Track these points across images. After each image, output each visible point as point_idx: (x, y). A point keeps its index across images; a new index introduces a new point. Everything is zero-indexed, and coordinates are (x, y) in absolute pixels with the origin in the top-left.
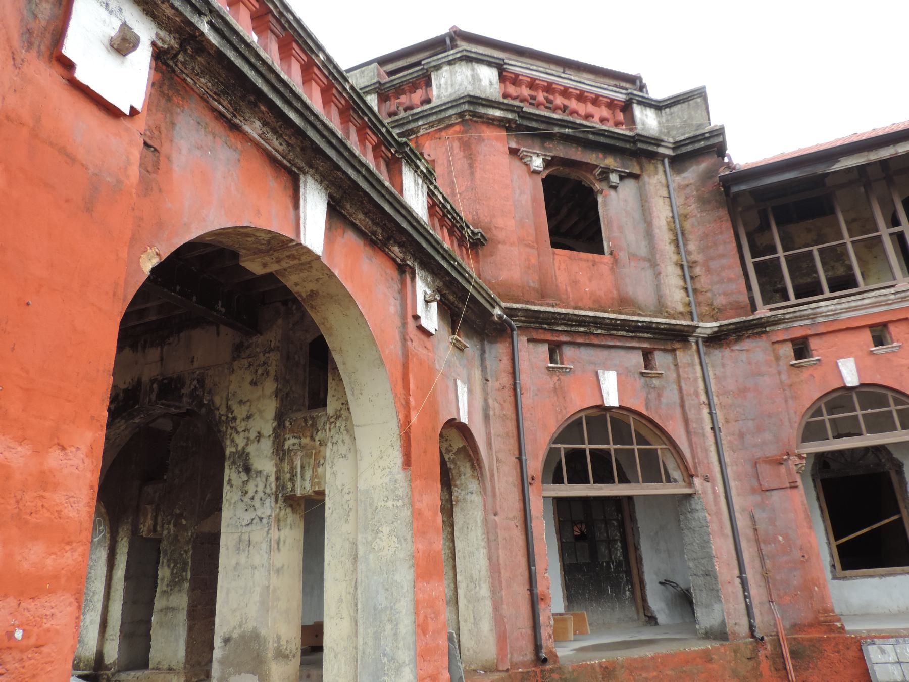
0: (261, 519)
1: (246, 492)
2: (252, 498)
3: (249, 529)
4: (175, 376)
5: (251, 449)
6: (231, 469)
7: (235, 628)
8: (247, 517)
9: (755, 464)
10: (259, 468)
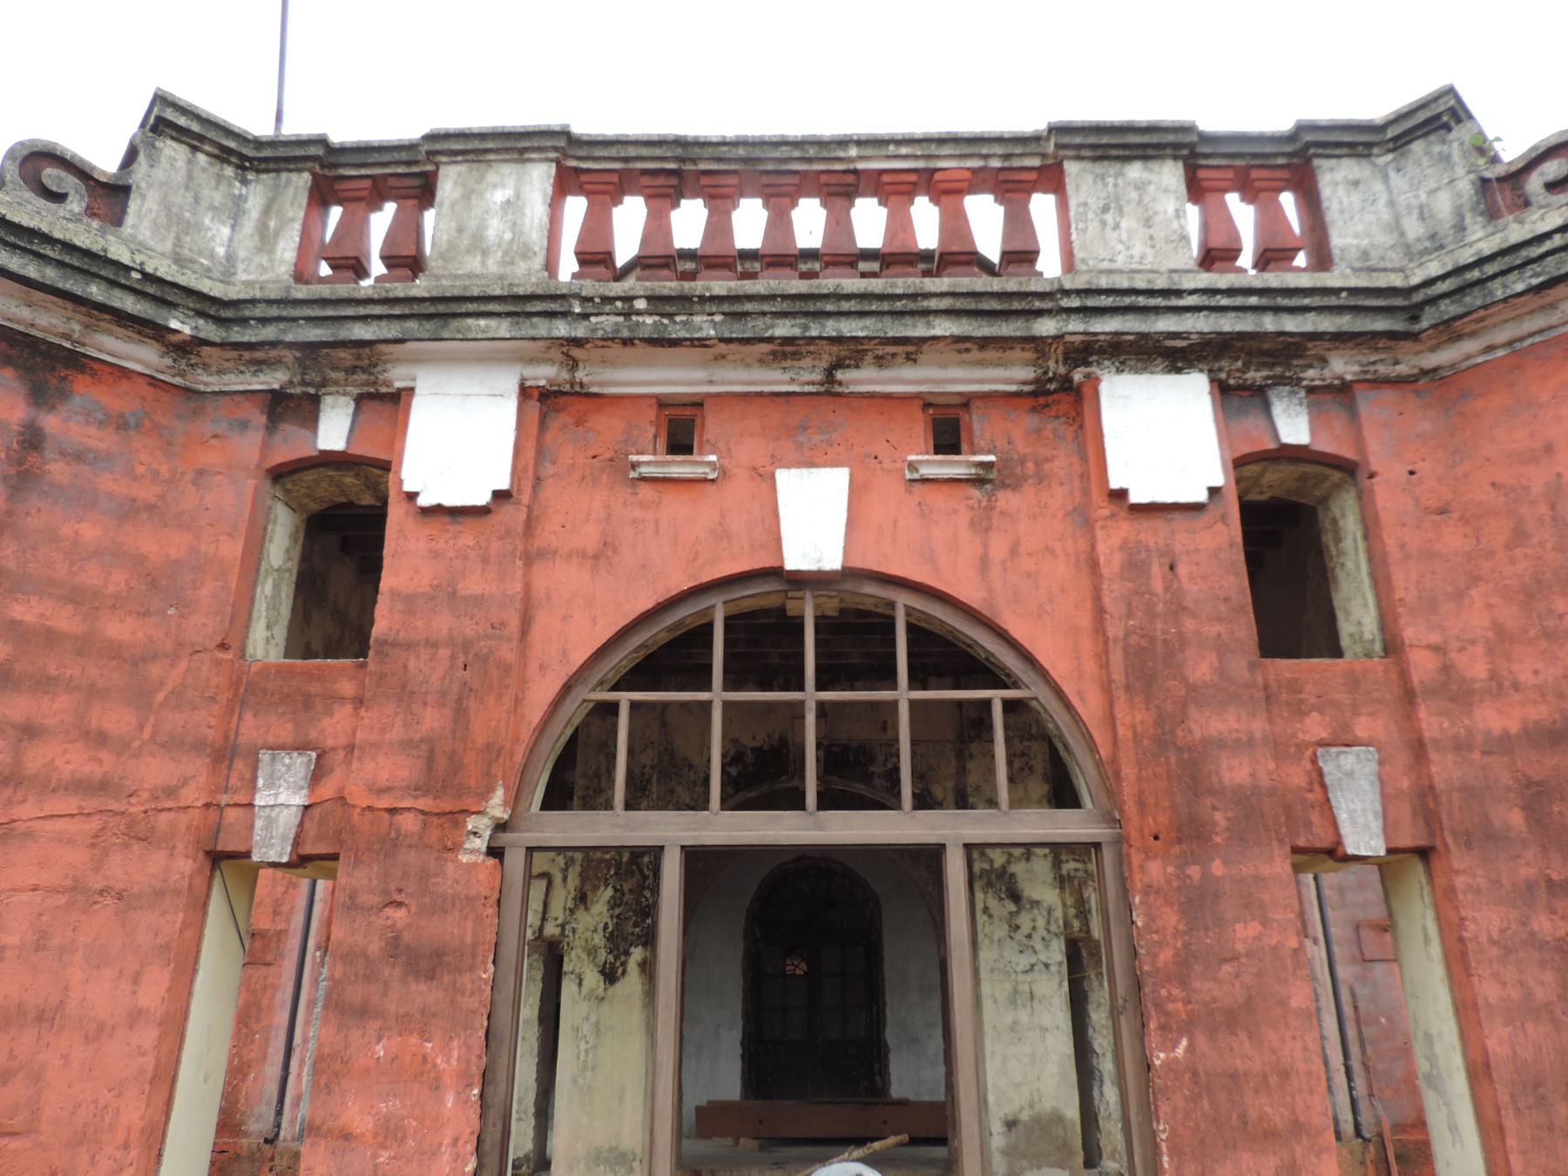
0: (1047, 966)
1: (1018, 927)
2: (1029, 936)
3: (1028, 977)
4: (854, 745)
5: (1017, 868)
6: (985, 893)
7: (1022, 1108)
8: (1024, 961)
9: (1357, 928)
10: (1036, 896)
